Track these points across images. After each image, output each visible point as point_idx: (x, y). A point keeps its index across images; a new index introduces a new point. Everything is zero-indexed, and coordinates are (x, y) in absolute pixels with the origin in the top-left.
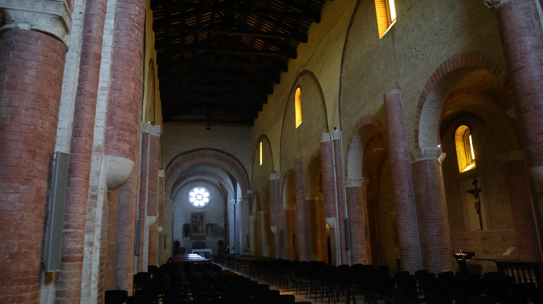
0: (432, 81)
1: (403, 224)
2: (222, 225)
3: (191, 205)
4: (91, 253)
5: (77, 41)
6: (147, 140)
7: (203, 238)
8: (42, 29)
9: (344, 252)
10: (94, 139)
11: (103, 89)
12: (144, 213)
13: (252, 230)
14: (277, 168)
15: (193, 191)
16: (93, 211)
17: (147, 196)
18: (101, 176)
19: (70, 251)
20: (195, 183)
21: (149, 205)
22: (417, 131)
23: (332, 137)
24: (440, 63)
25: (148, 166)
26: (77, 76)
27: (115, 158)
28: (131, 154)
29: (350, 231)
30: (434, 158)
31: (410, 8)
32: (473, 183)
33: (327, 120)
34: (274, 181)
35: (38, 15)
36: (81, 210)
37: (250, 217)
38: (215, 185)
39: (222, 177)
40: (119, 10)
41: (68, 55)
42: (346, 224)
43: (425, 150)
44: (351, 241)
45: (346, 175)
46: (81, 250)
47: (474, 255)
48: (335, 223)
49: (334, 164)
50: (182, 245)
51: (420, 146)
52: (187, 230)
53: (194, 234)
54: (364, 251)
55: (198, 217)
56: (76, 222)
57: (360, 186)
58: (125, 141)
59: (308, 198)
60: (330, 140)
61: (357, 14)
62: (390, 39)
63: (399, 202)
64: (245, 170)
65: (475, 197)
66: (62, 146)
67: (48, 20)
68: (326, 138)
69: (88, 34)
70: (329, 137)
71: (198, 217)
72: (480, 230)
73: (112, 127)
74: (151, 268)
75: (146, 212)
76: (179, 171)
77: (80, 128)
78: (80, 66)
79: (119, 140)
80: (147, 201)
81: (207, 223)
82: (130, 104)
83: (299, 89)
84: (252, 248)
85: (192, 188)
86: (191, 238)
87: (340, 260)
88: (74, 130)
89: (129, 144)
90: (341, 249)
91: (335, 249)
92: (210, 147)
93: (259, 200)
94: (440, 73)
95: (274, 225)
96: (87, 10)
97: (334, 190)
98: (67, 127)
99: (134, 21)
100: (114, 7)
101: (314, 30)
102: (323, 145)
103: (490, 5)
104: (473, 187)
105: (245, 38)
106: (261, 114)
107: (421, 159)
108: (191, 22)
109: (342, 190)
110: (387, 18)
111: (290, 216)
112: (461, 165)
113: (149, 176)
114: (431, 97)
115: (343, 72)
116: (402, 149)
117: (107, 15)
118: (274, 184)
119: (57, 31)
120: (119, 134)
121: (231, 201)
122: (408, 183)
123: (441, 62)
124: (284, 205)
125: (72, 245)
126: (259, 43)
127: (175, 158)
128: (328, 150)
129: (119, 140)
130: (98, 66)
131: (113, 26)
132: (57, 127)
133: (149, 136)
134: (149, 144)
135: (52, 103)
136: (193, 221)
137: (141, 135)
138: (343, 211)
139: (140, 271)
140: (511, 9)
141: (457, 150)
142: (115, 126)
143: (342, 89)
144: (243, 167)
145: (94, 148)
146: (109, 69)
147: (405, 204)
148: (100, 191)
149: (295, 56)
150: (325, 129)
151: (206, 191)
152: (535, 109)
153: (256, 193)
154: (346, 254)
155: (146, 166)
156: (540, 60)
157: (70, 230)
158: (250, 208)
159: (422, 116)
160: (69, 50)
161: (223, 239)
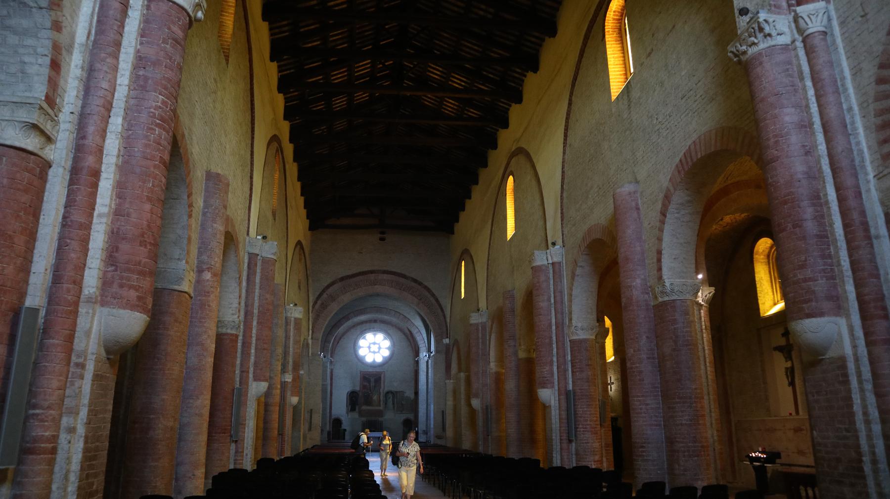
0: (679, 172)
1: (638, 403)
2: (410, 394)
3: (360, 360)
4: (70, 442)
5: (64, 152)
6: (256, 265)
7: (380, 413)
8: (8, 143)
9: (565, 445)
10: (84, 285)
11: (100, 215)
12: (248, 377)
13: (450, 403)
14: (483, 304)
15: (364, 338)
16: (77, 385)
17: (253, 351)
18: (93, 336)
19: (35, 440)
20: (368, 325)
22: (659, 253)
23: (550, 258)
24: (688, 144)
25: (256, 304)
26: (63, 200)
27: (114, 310)
29: (575, 411)
30: (689, 297)
31: (650, 54)
32: (783, 335)
34: (477, 325)
35: (4, 123)
36: (55, 384)
38: (400, 330)
39: (408, 316)
40: (132, 102)
41: (51, 172)
43: (672, 284)
44: (576, 428)
45: (571, 320)
46: (55, 438)
47: (780, 458)
48: (552, 398)
49: (552, 301)
50: (346, 425)
51: (665, 277)
52: (353, 400)
53: (364, 408)
54: (596, 445)
55: (372, 380)
56: (45, 400)
57: (594, 337)
58: (131, 287)
59: (522, 355)
61: (583, 59)
62: (626, 102)
63: (632, 368)
64: (440, 305)
65: (786, 358)
66: (36, 296)
67: (18, 129)
68: (541, 259)
69: (81, 142)
71: (372, 380)
72: (794, 413)
73: (113, 268)
74: (263, 463)
75: (251, 376)
76: (334, 307)
77: (67, 271)
78: (69, 185)
79: (121, 286)
80: (252, 359)
81: (386, 389)
82: (142, 235)
83: (511, 178)
84: (450, 433)
85: (362, 333)
86: (361, 414)
87: (559, 457)
88: (54, 275)
89: (137, 290)
92: (385, 268)
93: (457, 355)
94: (689, 160)
96: (83, 107)
97: (551, 344)
98: (43, 270)
99: (154, 116)
100: (125, 99)
101: (532, 83)
102: (536, 270)
103: (736, 56)
104: (782, 342)
105: (428, 99)
106: (463, 216)
107: (666, 299)
108: (338, 76)
110: (625, 67)
111: (499, 380)
112: (764, 304)
113: (258, 319)
114: (680, 197)
115: (567, 152)
116: (638, 281)
117: (113, 111)
118: (477, 329)
119: (31, 142)
120: (121, 278)
121: (423, 354)
122: (647, 337)
123: (689, 142)
124: (493, 365)
125: (41, 431)
126: (450, 105)
128: (543, 278)
129: (121, 286)
130: (95, 186)
131: (120, 127)
132: (29, 272)
133: (259, 257)
134: (258, 270)
135: (20, 241)
136: (364, 387)
139: (238, 467)
140: (761, 63)
141: (757, 279)
142: (117, 266)
143: (566, 181)
144: (437, 300)
146: (110, 187)
147: (640, 372)
148: (90, 357)
149: (505, 125)
150: (543, 245)
151: (385, 339)
152: (795, 226)
153: (456, 343)
154: (568, 448)
155: (253, 305)
156: (804, 146)
157: (37, 411)
158: (448, 367)
159: (667, 228)
160: (54, 166)
161: (411, 416)
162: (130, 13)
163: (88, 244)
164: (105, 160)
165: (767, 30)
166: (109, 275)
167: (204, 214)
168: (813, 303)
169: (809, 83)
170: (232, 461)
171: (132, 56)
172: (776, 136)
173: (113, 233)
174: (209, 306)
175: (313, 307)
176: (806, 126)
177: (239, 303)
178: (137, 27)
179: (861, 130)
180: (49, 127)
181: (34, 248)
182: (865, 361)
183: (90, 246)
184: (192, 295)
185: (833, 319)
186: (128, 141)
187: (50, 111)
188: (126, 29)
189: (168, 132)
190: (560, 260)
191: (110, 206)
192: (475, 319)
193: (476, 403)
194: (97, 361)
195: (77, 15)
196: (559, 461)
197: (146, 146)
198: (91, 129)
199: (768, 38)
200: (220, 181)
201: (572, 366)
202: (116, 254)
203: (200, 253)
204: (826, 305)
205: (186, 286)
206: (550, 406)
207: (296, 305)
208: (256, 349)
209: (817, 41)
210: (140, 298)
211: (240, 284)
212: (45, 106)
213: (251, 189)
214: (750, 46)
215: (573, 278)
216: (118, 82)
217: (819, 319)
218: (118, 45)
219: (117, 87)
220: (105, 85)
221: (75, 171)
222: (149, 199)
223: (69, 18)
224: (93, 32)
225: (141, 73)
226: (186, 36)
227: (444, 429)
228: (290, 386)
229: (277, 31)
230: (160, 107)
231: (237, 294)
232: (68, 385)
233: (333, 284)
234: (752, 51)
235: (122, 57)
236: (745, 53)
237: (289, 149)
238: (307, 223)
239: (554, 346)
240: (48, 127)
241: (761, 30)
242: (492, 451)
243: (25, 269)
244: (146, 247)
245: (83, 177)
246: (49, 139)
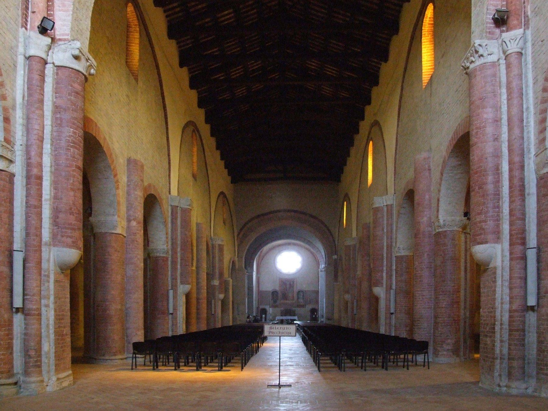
11: (46, 200)
17: (179, 267)
19: (29, 310)
21: (182, 274)
25: (179, 238)
28: (74, 245)
34: (349, 246)
40: (55, 134)
41: (15, 179)
43: (444, 221)
46: (39, 309)
49: (385, 231)
58: (68, 237)
75: (179, 281)
76: (253, 237)
77: (32, 231)
82: (71, 209)
93: (336, 268)
102: (377, 210)
107: (440, 230)
113: (181, 247)
115: (400, 126)
116: (425, 219)
120: (62, 232)
129: (62, 236)
130: (41, 185)
133: (179, 208)
137: (170, 208)
144: (329, 230)
145: (43, 243)
146: (49, 184)
147: (421, 276)
152: (480, 188)
157: (28, 297)
162: (46, 79)
163: (41, 215)
164: (44, 169)
165: (481, 51)
166: (55, 231)
167: (128, 186)
168: (483, 236)
169: (504, 90)
170: (170, 330)
171: (51, 107)
172: (477, 128)
173: (54, 209)
174: (137, 241)
176: (497, 121)
177: (167, 238)
178: (51, 88)
179: (532, 123)
180: (9, 155)
181: (13, 219)
182: (507, 269)
183: (43, 216)
184: (125, 235)
185: (493, 245)
186: (56, 157)
187: (8, 146)
188: (45, 90)
189: (79, 150)
191: (50, 195)
194: (55, 274)
195: (15, 87)
197: (67, 159)
198: (33, 154)
199: (481, 57)
200: (137, 164)
202: (57, 220)
203: (128, 210)
204: (490, 237)
205: (119, 231)
208: (181, 265)
209: (514, 60)
210: (73, 242)
211: (166, 226)
212: (5, 144)
213: (169, 163)
214: (471, 63)
216: (45, 123)
217: (484, 245)
218: (42, 101)
219: (45, 127)
220: (37, 127)
221: (28, 177)
222: (72, 189)
223: (10, 90)
224: (26, 94)
225: (58, 116)
226: (84, 89)
229: (182, 44)
230: (72, 136)
231: (164, 232)
232: (42, 285)
234: (472, 66)
235: (45, 108)
236: (468, 68)
237: (205, 129)
238: (229, 179)
239: (385, 260)
240: (9, 155)
241: (477, 52)
242: (356, 327)
243: (11, 230)
244: (73, 215)
245: (34, 180)
246: (11, 161)
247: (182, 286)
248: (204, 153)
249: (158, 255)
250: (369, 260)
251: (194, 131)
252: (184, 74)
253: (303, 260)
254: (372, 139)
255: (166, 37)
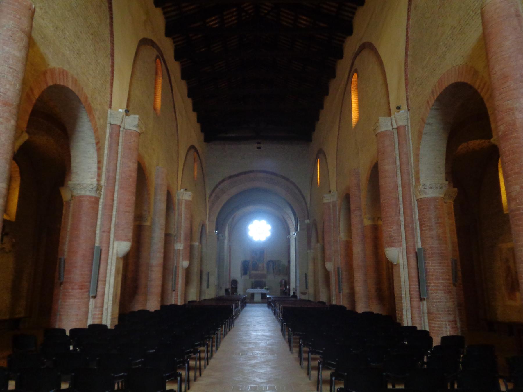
9: (416, 303)
13: (311, 267)
33: (389, 103)
37: (309, 251)
42: (419, 257)
45: (418, 179)
48: (401, 257)
53: (253, 272)
57: (442, 196)
60: (391, 128)
63: (518, 209)
64: (303, 196)
70: (389, 124)
76: (225, 198)
86: (251, 277)
87: (409, 316)
90: (411, 298)
91: (401, 297)
93: (314, 232)
95: (330, 260)
97: (397, 204)
109: (411, 204)
115: (411, 16)
127: (220, 183)
138: (414, 238)
143: (410, 46)
144: (300, 192)
154: (419, 307)
175: (210, 198)
190: (406, 124)
192: (328, 199)
193: (329, 266)
196: (410, 320)
201: (420, 225)
206: (398, 265)
207: (186, 190)
215: (420, 137)
227: (307, 288)
228: (181, 252)
233: (223, 181)
247: (116, 244)
248: (172, 92)
249: (83, 193)
250: (361, 215)
251: (157, 57)
252: (189, 102)
253: (273, 227)
254: (356, 71)
255: (154, 7)
